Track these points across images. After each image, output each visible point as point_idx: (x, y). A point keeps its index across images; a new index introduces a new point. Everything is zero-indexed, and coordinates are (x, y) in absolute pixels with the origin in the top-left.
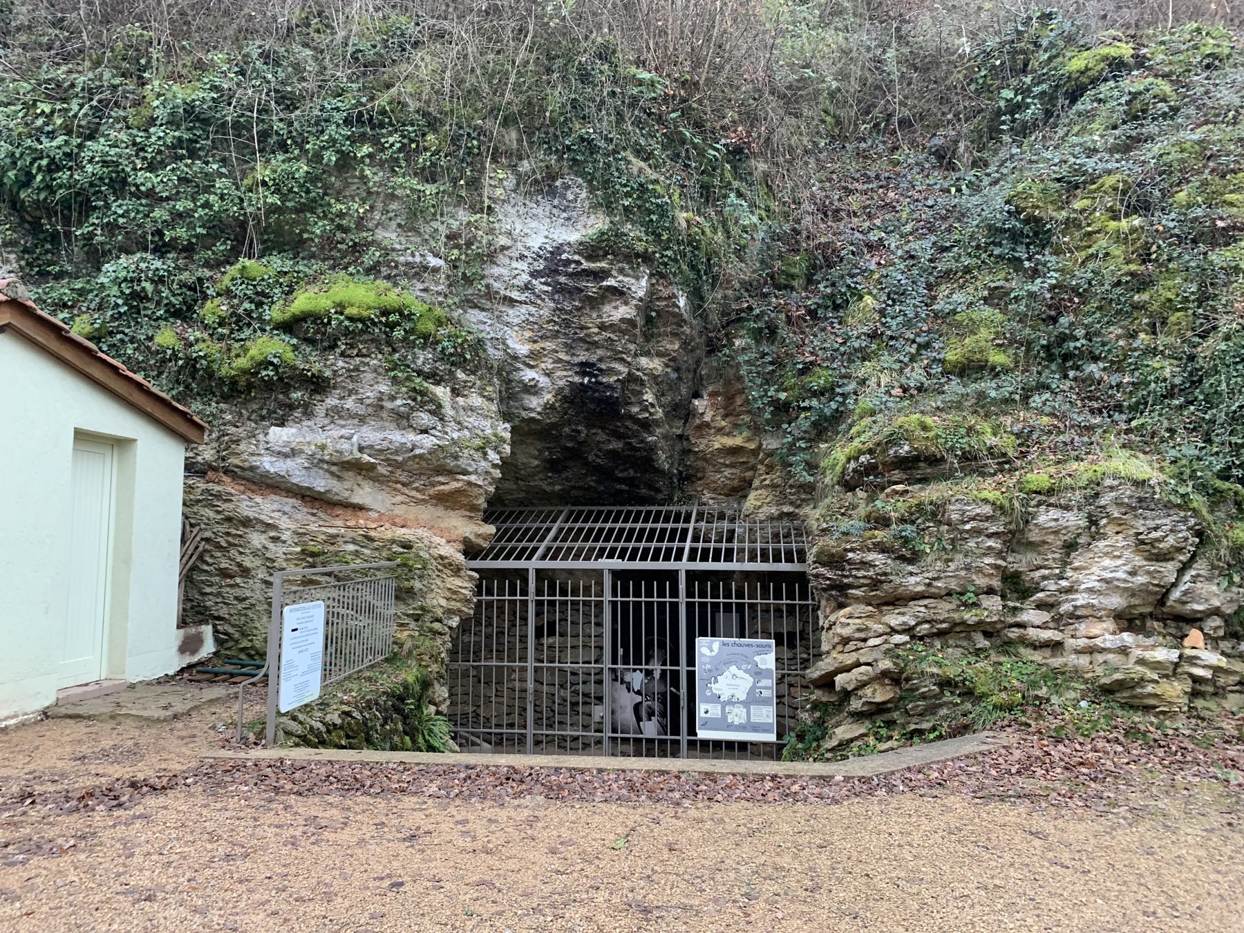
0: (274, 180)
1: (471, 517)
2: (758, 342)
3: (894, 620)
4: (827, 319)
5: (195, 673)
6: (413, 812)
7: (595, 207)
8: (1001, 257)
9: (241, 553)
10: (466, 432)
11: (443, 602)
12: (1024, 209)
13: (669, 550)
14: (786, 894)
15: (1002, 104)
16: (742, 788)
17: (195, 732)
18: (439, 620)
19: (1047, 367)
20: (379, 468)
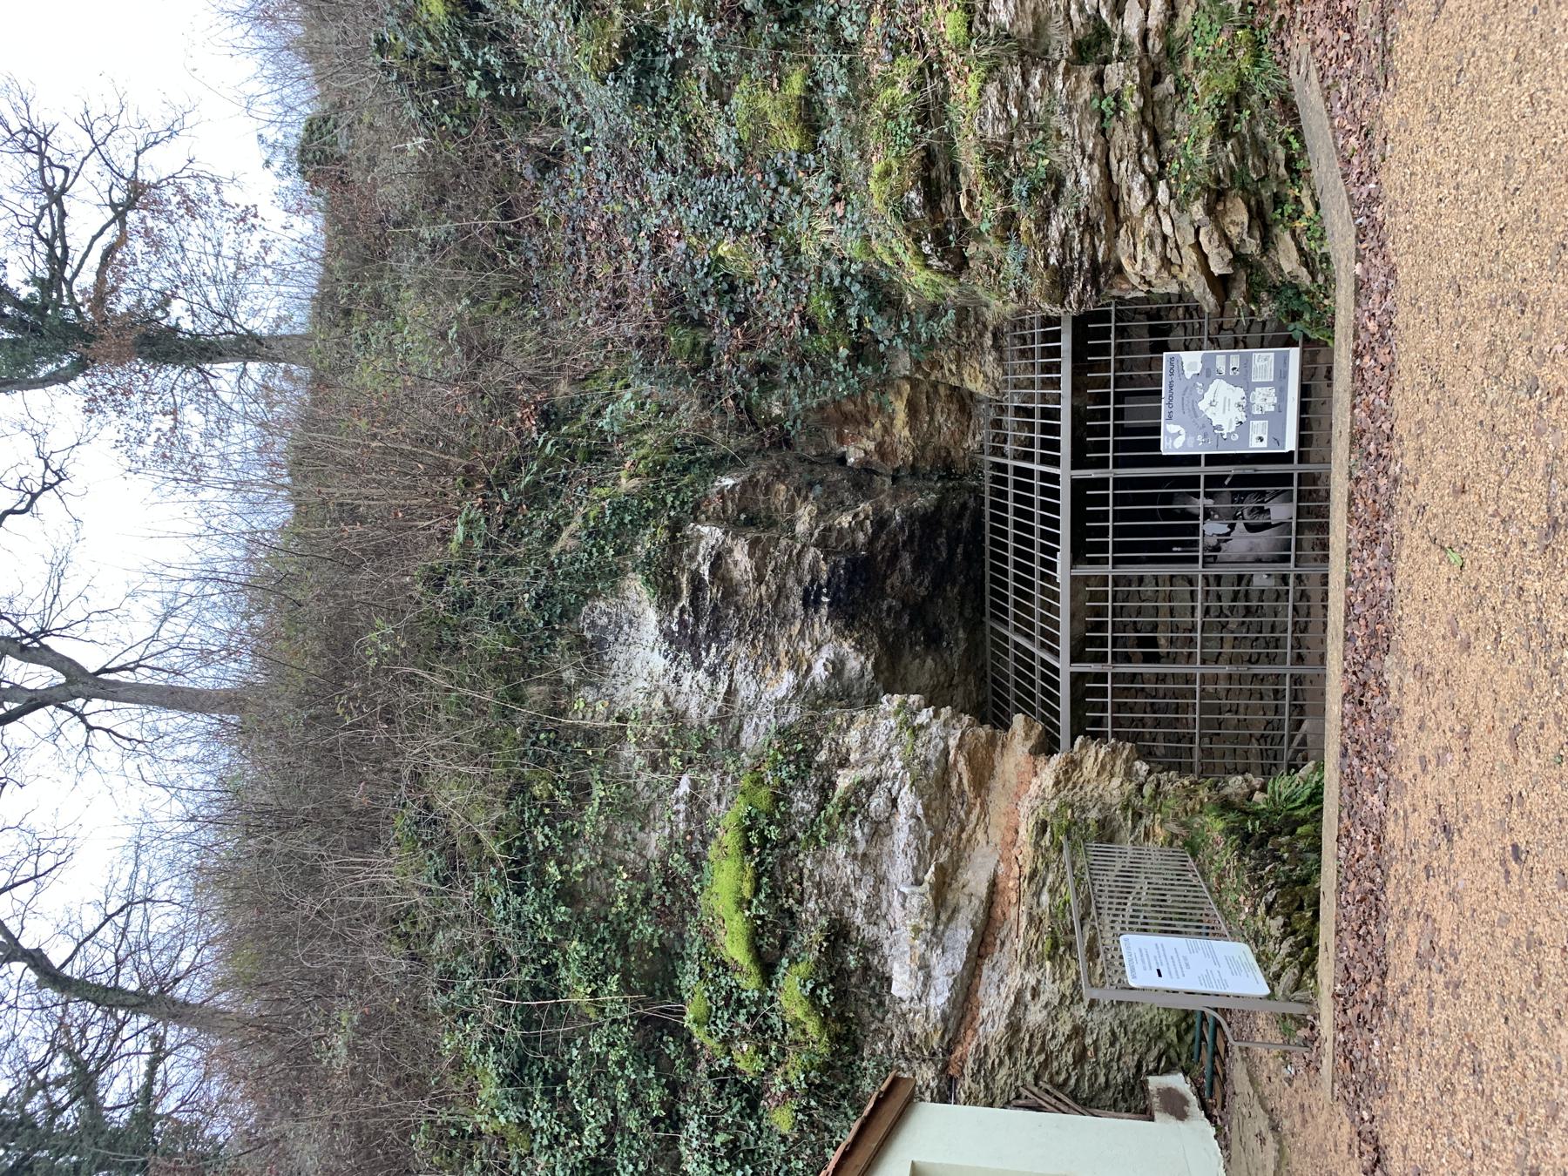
0: (590, 981)
1: (1003, 746)
2: (775, 386)
3: (1137, 201)
4: (747, 300)
5: (1214, 1100)
6: (1409, 827)
7: (616, 590)
8: (670, 86)
9: (1054, 1037)
10: (894, 750)
11: (1116, 782)
12: (613, 62)
13: (1044, 491)
14: (1529, 339)
15: (483, 94)
16: (1372, 396)
17: (1296, 1105)
18: (1140, 787)
19: (807, 21)
20: (941, 860)
